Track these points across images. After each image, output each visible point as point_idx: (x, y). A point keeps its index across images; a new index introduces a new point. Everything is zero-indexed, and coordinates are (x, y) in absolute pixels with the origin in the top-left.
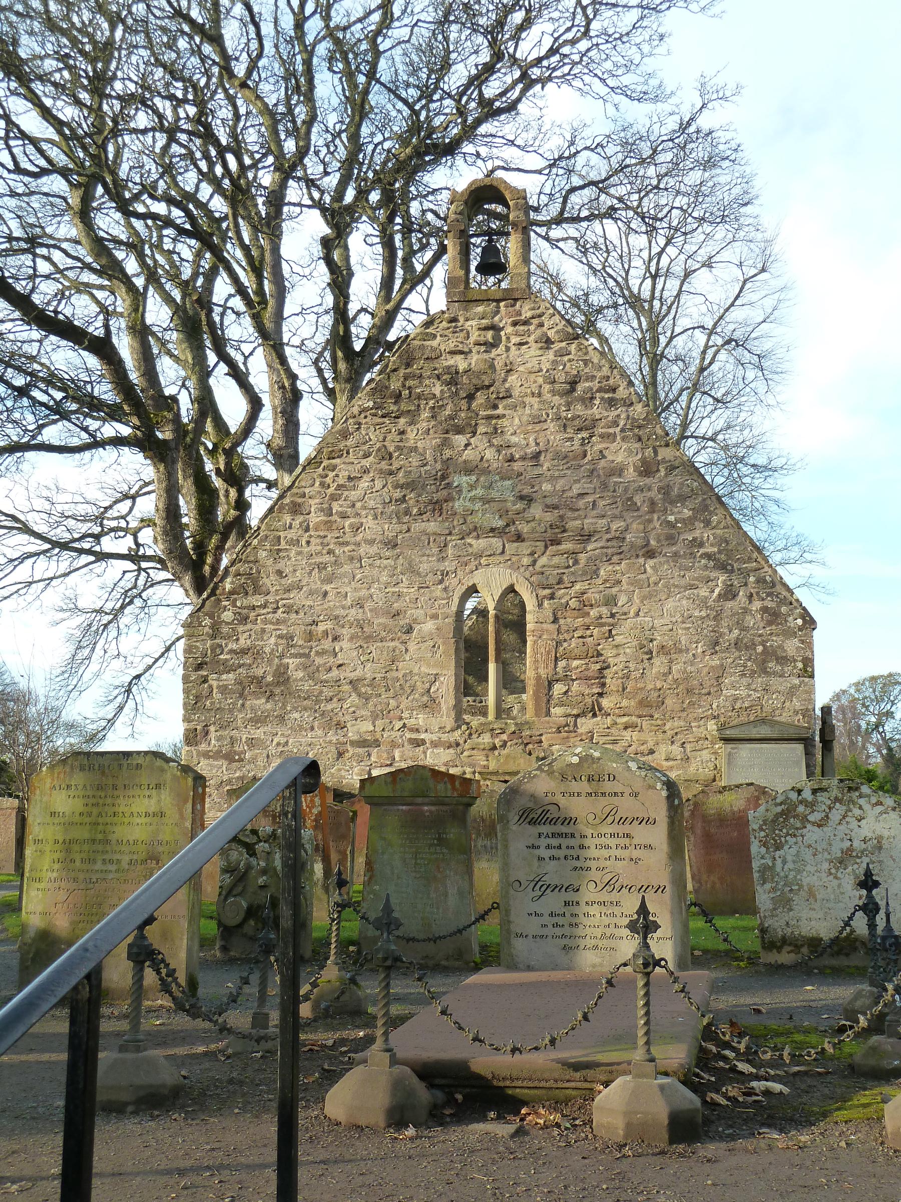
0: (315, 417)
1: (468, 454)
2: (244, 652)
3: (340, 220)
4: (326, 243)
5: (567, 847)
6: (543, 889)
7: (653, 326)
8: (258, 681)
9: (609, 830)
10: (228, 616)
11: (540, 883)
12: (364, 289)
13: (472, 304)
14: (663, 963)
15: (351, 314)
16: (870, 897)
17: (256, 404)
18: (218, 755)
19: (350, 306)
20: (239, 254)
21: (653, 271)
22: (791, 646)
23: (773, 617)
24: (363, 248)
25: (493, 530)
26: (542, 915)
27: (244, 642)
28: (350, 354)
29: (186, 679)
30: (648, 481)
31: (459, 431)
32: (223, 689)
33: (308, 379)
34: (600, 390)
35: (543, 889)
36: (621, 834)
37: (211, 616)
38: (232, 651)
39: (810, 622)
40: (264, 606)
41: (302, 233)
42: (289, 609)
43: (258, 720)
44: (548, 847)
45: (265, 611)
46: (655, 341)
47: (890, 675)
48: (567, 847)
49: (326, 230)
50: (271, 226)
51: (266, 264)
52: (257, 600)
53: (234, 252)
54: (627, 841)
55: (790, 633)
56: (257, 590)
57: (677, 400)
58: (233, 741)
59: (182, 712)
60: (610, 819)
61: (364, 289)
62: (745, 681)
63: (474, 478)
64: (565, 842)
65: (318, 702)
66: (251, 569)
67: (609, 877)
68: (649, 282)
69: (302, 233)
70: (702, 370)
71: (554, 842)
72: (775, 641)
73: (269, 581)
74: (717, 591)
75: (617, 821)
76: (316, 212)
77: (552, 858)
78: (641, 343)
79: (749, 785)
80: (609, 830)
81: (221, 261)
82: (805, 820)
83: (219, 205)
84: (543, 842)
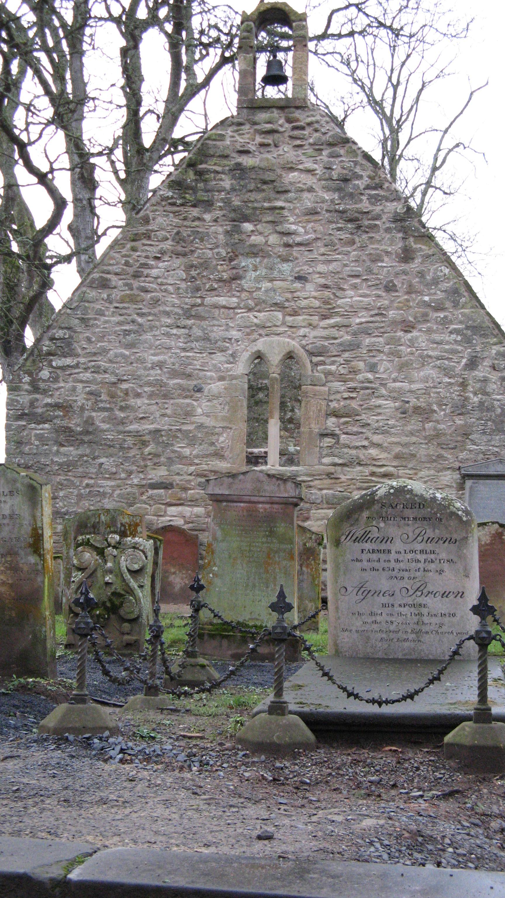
1: (255, 239)
2: (57, 406)
3: (132, 30)
4: (124, 52)
5: (389, 561)
6: (365, 594)
7: (395, 132)
8: (67, 430)
9: (418, 547)
10: (45, 374)
11: (363, 589)
13: (258, 111)
14: (498, 637)
15: (141, 114)
17: (60, 204)
19: (141, 109)
21: (395, 82)
25: (276, 304)
26: (363, 614)
28: (141, 150)
29: (8, 427)
30: (404, 266)
31: (246, 219)
32: (40, 437)
34: (368, 187)
35: (365, 594)
36: (428, 551)
37: (30, 374)
38: (47, 405)
41: (104, 44)
44: (369, 561)
45: (77, 371)
46: (396, 143)
48: (385, 561)
49: (123, 43)
52: (68, 361)
54: (432, 556)
56: (72, 354)
57: (412, 195)
59: (4, 422)
60: (420, 539)
62: (485, 438)
63: (258, 260)
64: (383, 557)
66: (65, 334)
67: (419, 584)
68: (391, 90)
69: (104, 44)
70: (435, 169)
71: (374, 556)
74: (464, 361)
75: (426, 539)
76: (112, 26)
78: (384, 143)
79: (493, 523)
80: (418, 547)
84: (365, 557)
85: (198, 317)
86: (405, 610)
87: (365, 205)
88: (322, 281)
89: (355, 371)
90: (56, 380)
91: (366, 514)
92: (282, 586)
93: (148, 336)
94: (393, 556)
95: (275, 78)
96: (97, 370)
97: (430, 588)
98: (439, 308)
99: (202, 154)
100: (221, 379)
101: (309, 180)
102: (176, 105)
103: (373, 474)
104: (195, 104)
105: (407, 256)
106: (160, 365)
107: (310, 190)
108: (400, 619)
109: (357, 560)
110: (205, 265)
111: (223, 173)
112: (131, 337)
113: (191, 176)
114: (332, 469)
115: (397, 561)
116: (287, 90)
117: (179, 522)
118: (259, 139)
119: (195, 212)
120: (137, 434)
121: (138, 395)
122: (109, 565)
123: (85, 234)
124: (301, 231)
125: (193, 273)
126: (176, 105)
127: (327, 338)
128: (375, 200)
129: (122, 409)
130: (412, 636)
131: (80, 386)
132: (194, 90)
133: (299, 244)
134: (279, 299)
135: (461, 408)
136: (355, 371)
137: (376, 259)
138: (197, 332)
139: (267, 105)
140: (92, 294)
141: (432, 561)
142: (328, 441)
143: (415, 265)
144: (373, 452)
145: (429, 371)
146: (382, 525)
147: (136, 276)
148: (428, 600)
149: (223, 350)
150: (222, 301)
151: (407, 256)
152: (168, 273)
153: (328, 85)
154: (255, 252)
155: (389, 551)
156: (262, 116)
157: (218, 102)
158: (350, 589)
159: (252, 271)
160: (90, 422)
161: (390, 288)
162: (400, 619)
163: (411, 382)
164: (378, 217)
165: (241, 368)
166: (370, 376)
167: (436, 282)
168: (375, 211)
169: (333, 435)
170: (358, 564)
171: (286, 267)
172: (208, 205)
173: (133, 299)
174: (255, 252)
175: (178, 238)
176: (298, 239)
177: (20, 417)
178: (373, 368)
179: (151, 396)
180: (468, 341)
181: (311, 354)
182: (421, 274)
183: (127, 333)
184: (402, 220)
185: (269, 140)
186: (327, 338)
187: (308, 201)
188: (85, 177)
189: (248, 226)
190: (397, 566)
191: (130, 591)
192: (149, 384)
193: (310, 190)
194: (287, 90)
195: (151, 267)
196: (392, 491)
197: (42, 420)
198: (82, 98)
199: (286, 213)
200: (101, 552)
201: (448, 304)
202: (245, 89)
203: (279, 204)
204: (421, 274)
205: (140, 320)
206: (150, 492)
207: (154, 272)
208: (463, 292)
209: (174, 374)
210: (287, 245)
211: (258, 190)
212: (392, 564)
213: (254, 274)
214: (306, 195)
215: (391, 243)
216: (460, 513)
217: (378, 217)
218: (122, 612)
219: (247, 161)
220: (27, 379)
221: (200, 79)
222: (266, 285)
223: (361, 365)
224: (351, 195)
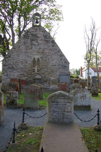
0: (16, 38)
2: (9, 64)
12: (22, 23)
16: (98, 113)
17: (10, 36)
18: (6, 75)
20: (9, 20)
22: (67, 65)
23: (65, 62)
24: (22, 19)
27: (9, 63)
29: (2, 67)
31: (33, 40)
32: (6, 68)
33: (16, 34)
39: (69, 63)
40: (11, 59)
41: (16, 17)
42: (14, 60)
43: (10, 72)
47: (69, 62)
50: (12, 17)
51: (11, 21)
52: (10, 58)
53: (8, 19)
55: (67, 64)
56: (10, 57)
58: (8, 74)
59: (2, 66)
61: (22, 23)
65: (17, 70)
69: (16, 17)
70: (54, 35)
71: (56, 105)
72: (65, 65)
73: (12, 56)
77: (55, 107)
80: (64, 104)
81: (6, 20)
82: (78, 92)
83: (7, 14)
84: (54, 105)
85: (27, 53)
86: (61, 115)
87: (48, 39)
88: (43, 49)
89: (46, 60)
90: (8, 61)
91: (54, 98)
92: (42, 147)
93: (20, 55)
94: (59, 105)
95: (37, 22)
96: (14, 60)
97: (65, 111)
98: (57, 53)
99: (28, 31)
100: (30, 61)
101: (41, 36)
102: (25, 27)
103: (48, 73)
104: (27, 26)
105: (53, 46)
106: (22, 59)
107: (41, 37)
108: (60, 116)
109: (53, 106)
110: (28, 46)
111: (30, 34)
112: (18, 56)
113: (26, 35)
114: (43, 73)
115: (60, 106)
116: (38, 24)
117: (24, 79)
118: (35, 30)
119: (27, 39)
120: (19, 68)
121: (19, 63)
122: (12, 96)
123: (13, 40)
124: (40, 42)
125: (26, 47)
126: (25, 27)
127: (43, 56)
128: (50, 39)
129: (17, 65)
130: (62, 119)
131: (12, 62)
132: (27, 24)
133: (40, 44)
134: (37, 51)
135: (59, 65)
136: (46, 60)
137: (50, 46)
138: (27, 55)
139: (36, 26)
140: (13, 50)
141: (66, 106)
142: (43, 69)
143: (54, 47)
144: (49, 71)
145: (56, 61)
146: (57, 100)
147: (19, 47)
148: (65, 113)
149: (30, 57)
150: (30, 51)
151: (53, 46)
152: (23, 47)
153: (43, 24)
154: (34, 45)
155: (58, 104)
156: (36, 27)
157: (29, 26)
158: (51, 111)
159: (34, 48)
160: (13, 66)
161: (51, 50)
162: (60, 116)
163: (54, 62)
164: (50, 41)
165: (32, 60)
166: (48, 61)
167: (57, 49)
168: (49, 40)
169: (44, 68)
170: (53, 107)
171: (38, 47)
172: (28, 39)
173: (18, 50)
174: (34, 45)
175: (24, 43)
176: (40, 43)
177: (4, 66)
178: (49, 60)
179: (21, 63)
180: (60, 57)
181: (41, 58)
182: (55, 48)
183: (17, 55)
184: (53, 41)
185: (36, 30)
186: (43, 56)
187: (41, 38)
188: (13, 35)
189: (33, 42)
190: (60, 107)
191: (15, 100)
192: (20, 61)
193: (41, 37)
194: (38, 24)
195: (21, 46)
196: (59, 93)
197: (7, 66)
198: (13, 24)
199: (38, 40)
200: (10, 94)
201: (58, 52)
202: (33, 24)
203: (38, 39)
204: (55, 48)
205: (19, 53)
206: (21, 75)
207: (21, 47)
208: (59, 51)
209: (24, 60)
210: (38, 44)
211: (35, 37)
212: (59, 107)
213: (34, 48)
214: (40, 38)
215: (51, 44)
216: (71, 98)
217: (50, 41)
218: (14, 103)
219: (34, 33)
220: (5, 61)
221: (28, 23)
222: (35, 49)
223: (47, 60)
224: (47, 38)
